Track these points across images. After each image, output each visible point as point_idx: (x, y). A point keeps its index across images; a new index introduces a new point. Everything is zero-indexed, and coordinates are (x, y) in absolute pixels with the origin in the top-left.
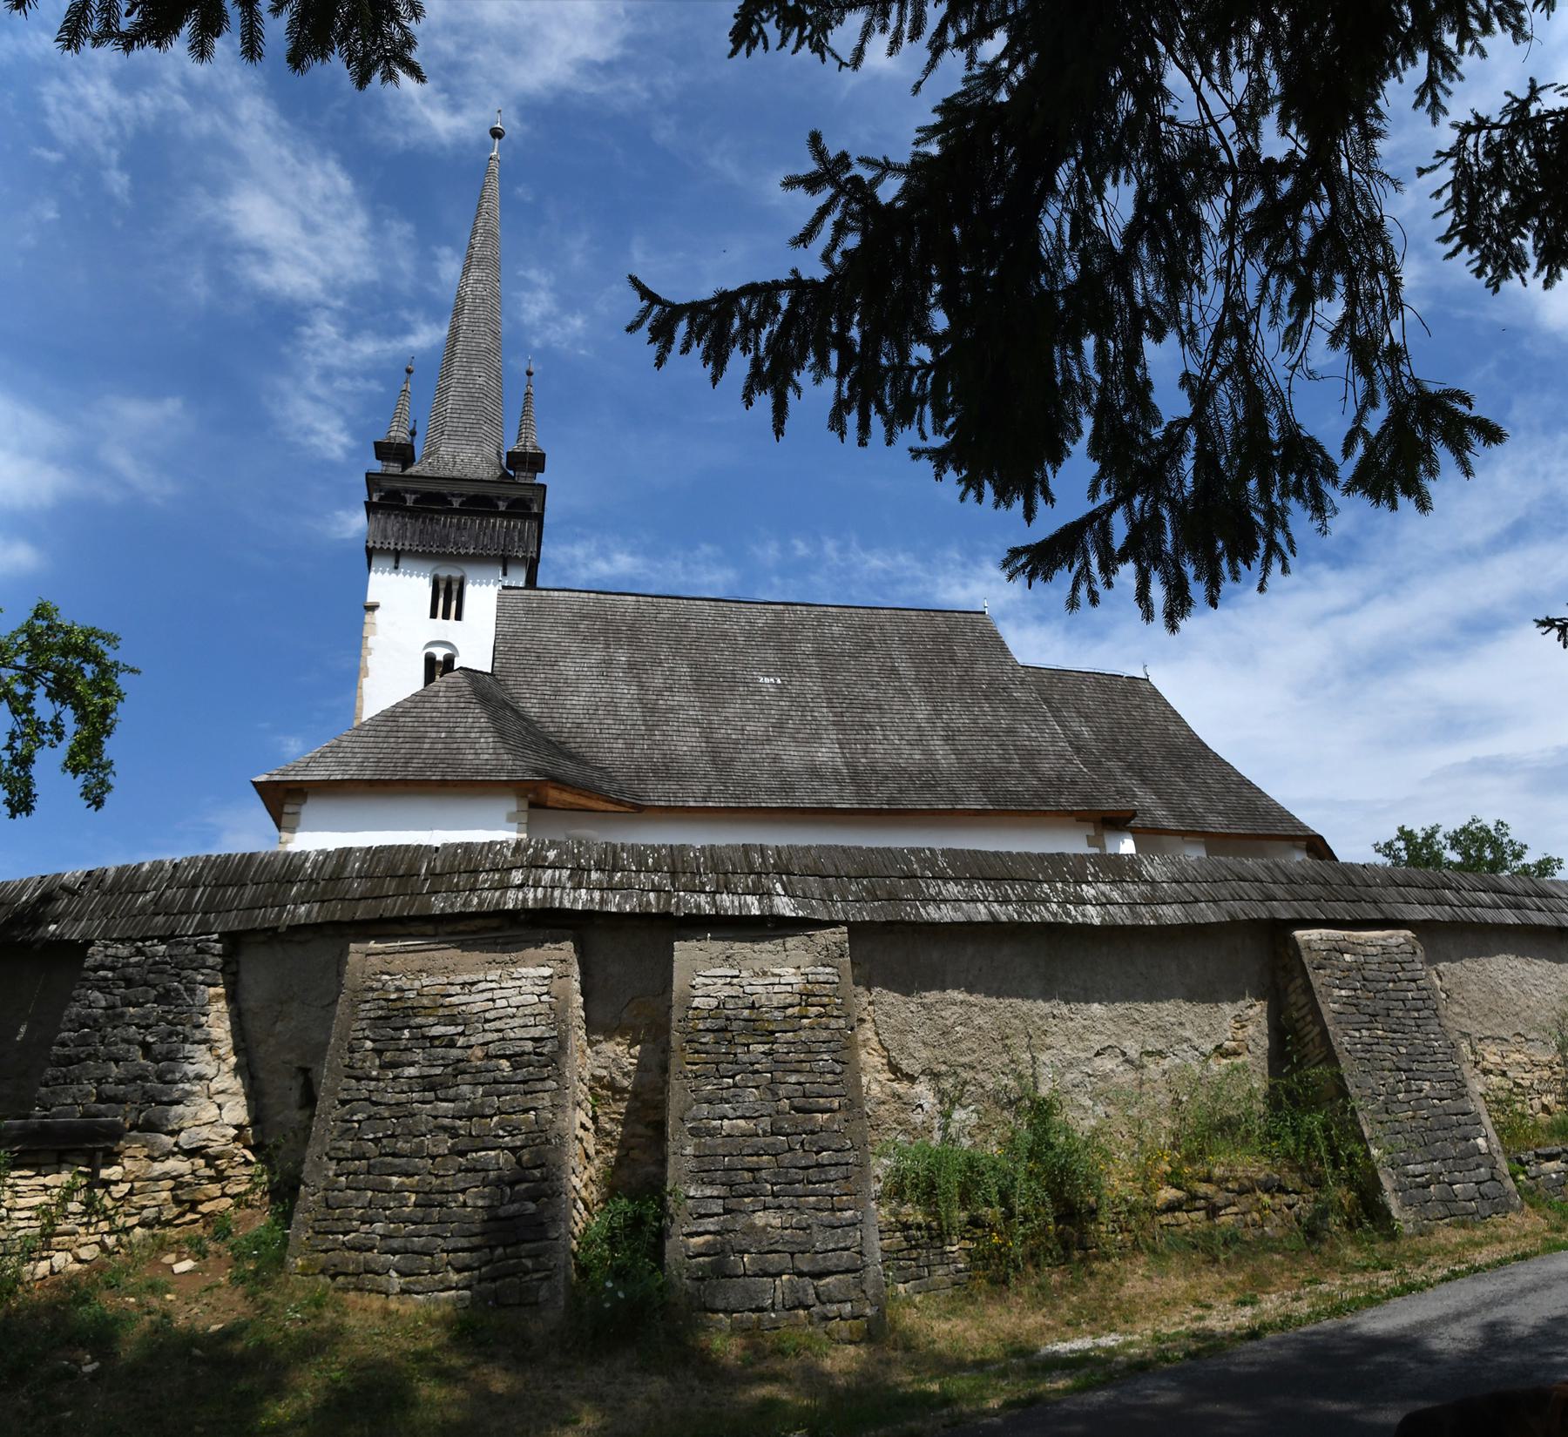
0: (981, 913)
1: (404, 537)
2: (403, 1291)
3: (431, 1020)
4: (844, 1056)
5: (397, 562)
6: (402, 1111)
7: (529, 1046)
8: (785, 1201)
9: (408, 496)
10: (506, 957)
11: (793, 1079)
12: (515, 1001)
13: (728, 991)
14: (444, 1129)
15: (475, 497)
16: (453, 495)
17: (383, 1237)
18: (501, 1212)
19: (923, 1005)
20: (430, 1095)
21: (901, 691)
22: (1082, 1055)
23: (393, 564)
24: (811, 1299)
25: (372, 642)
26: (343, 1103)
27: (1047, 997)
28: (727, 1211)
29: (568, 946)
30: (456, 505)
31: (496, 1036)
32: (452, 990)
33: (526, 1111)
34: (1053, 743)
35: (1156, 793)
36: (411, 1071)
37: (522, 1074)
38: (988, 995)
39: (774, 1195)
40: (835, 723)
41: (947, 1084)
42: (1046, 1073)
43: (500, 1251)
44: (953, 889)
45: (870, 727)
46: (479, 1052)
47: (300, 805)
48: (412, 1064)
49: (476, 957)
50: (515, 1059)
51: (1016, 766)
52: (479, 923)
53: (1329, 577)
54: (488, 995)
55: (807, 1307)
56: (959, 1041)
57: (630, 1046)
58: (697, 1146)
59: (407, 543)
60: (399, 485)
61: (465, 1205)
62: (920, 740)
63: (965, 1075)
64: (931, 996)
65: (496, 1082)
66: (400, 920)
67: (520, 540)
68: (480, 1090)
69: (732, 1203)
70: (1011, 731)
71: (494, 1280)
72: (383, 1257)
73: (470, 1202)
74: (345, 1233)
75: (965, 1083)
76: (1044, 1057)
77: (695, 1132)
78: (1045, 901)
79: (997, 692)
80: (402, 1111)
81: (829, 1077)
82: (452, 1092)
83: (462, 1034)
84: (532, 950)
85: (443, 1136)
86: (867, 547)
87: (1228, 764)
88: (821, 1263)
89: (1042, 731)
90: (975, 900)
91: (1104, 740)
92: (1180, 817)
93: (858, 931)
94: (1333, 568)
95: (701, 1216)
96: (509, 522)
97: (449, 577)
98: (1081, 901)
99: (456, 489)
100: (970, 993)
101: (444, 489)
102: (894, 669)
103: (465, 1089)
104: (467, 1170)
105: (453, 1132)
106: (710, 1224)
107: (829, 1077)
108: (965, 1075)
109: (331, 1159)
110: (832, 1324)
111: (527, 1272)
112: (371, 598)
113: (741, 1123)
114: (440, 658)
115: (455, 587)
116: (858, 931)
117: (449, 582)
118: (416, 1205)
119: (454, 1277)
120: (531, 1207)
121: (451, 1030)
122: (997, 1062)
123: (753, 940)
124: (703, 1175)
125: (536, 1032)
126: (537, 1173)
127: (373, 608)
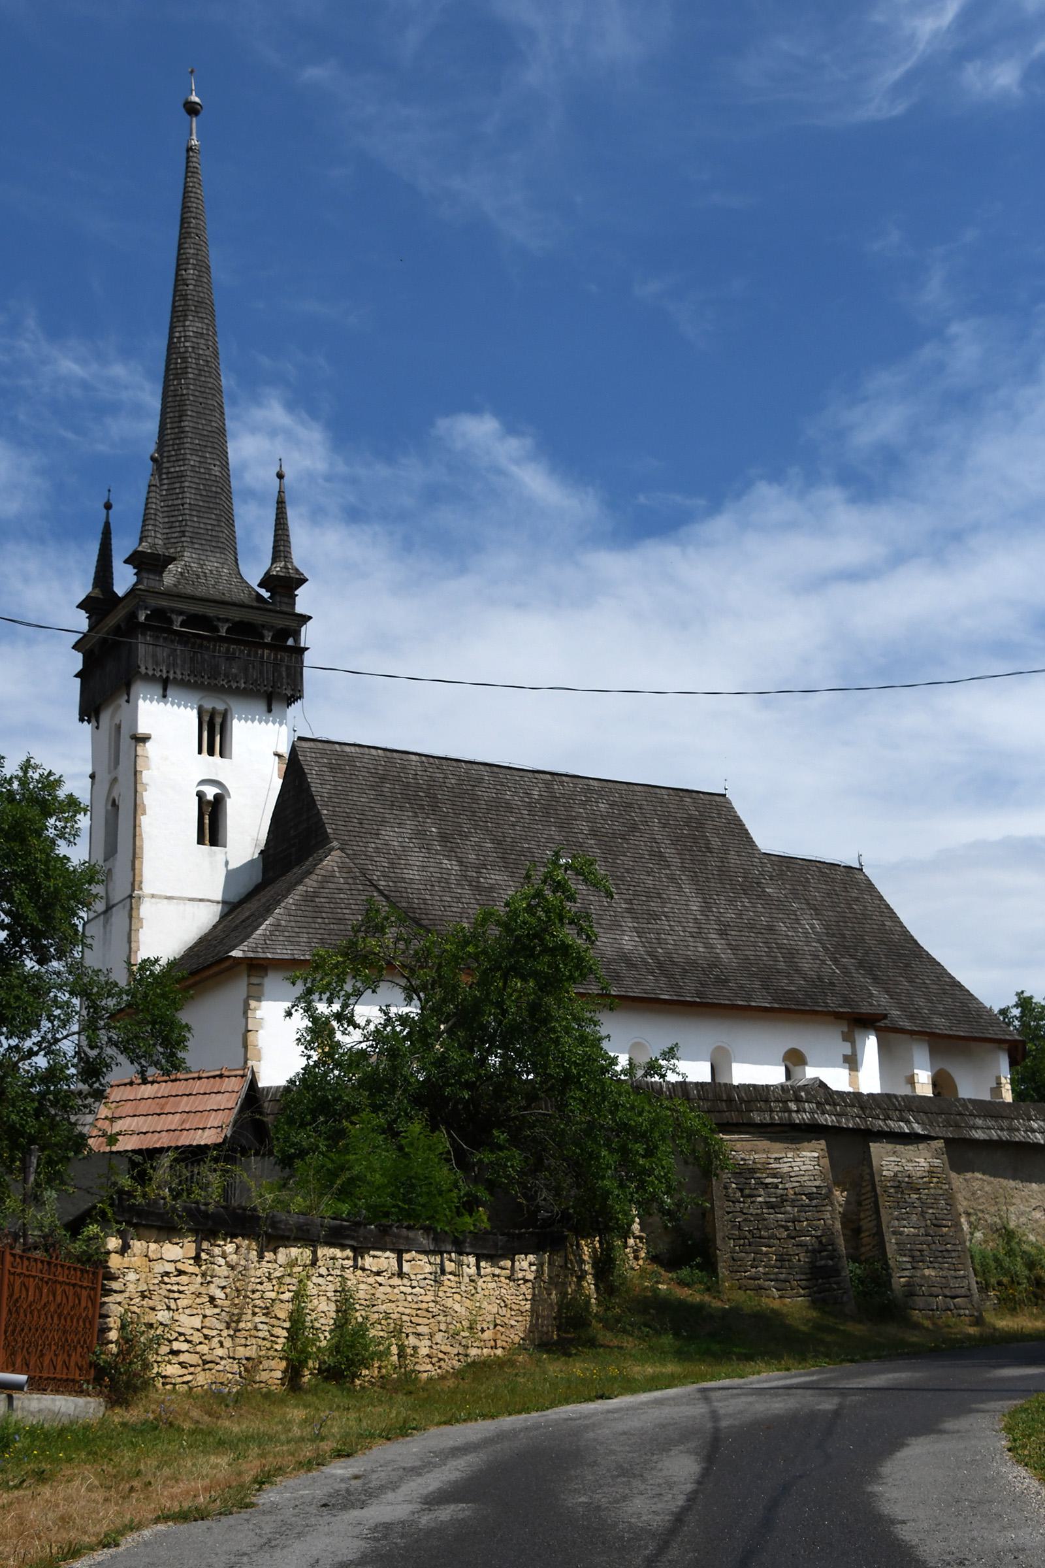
0: (994, 1135)
1: (175, 665)
2: (780, 1297)
3: (764, 1175)
4: (950, 1202)
5: (165, 690)
6: (760, 1218)
7: (814, 1190)
8: (936, 1265)
9: (174, 617)
10: (794, 1146)
11: (930, 1211)
12: (803, 1168)
13: (897, 1169)
14: (782, 1226)
15: (241, 622)
16: (219, 619)
17: (764, 1274)
18: (818, 1264)
19: (965, 1180)
20: (772, 1211)
21: (672, 879)
22: (1028, 1209)
23: (160, 691)
24: (952, 1307)
25: (146, 776)
26: (728, 1213)
27: (1014, 1180)
28: (914, 1268)
29: (823, 1142)
30: (223, 633)
31: (797, 1184)
32: (772, 1161)
33: (819, 1220)
34: (808, 943)
35: (887, 992)
36: (760, 1199)
37: (814, 1202)
38: (991, 1176)
39: (931, 1262)
40: (629, 911)
41: (973, 1219)
42: (1013, 1217)
43: (820, 1281)
44: (979, 1122)
45: (655, 917)
46: (791, 1192)
47: (263, 977)
48: (760, 1196)
49: (778, 1145)
50: (810, 1196)
51: (782, 965)
52: (778, 1129)
53: (845, 515)
54: (789, 1164)
55: (951, 1310)
56: (978, 1198)
57: (842, 1192)
58: (896, 1239)
59: (178, 672)
60: (164, 603)
61: (799, 1260)
62: (698, 935)
63: (980, 1215)
64: (969, 1175)
65: (802, 1206)
66: (737, 1125)
67: (288, 676)
68: (796, 1209)
69: (915, 1265)
70: (771, 929)
71: (820, 1293)
72: (767, 1283)
73: (802, 1259)
74: (745, 1272)
75: (980, 1219)
76: (1012, 1209)
77: (894, 1233)
78: (1018, 1130)
79: (751, 887)
80: (760, 1218)
81: (945, 1212)
82: (783, 1210)
83: (781, 1183)
84: (806, 1144)
85: (782, 1230)
86: (55, 332)
87: (939, 964)
88: (954, 1292)
89: (795, 930)
90: (989, 1128)
91: (833, 935)
92: (911, 1017)
93: (948, 1141)
94: (853, 500)
95: (904, 1269)
96: (276, 655)
97: (214, 709)
98: (1033, 1131)
99: (223, 613)
100: (984, 1174)
101: (211, 612)
102: (661, 855)
103: (789, 1208)
104: (797, 1246)
105: (787, 1229)
106: (907, 1273)
107: (945, 1212)
108: (980, 1215)
109: (730, 1239)
110: (963, 1318)
111: (835, 1290)
112: (142, 729)
113: (912, 1230)
114: (210, 797)
115: (218, 720)
116: (948, 1141)
117: (213, 714)
118: (776, 1260)
119: (802, 1292)
120: (831, 1263)
121: (776, 1180)
122: (993, 1209)
123: (905, 1144)
124: (901, 1252)
125: (817, 1183)
126: (830, 1247)
127: (145, 739)
